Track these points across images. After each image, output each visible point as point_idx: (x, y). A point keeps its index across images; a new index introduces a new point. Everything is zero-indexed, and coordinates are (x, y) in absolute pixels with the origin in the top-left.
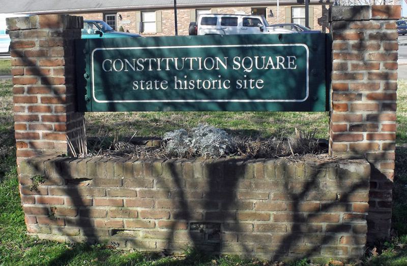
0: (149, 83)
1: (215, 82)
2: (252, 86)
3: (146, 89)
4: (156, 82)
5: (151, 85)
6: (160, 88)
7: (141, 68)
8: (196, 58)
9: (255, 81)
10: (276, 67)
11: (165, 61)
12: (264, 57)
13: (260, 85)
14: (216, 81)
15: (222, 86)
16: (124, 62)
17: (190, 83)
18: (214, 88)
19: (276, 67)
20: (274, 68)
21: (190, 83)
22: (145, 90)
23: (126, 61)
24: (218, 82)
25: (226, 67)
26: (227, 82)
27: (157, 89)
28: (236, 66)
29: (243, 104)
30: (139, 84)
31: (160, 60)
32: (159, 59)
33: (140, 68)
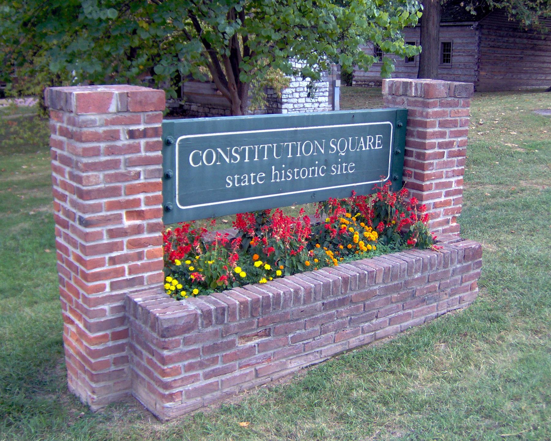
0: (245, 177)
1: (312, 170)
2: (254, 182)
3: (241, 186)
4: (252, 175)
5: (247, 179)
6: (257, 183)
7: (236, 159)
8: (270, 145)
9: (256, 176)
10: (366, 147)
11: (264, 148)
12: (228, 148)
13: (261, 179)
14: (313, 168)
15: (318, 173)
16: (314, 144)
17: (288, 174)
18: (310, 176)
19: (366, 147)
20: (364, 149)
21: (288, 174)
22: (276, 182)
23: (219, 150)
24: (315, 169)
25: (323, 151)
26: (323, 168)
27: (253, 183)
28: (333, 149)
29: (93, 212)
30: (337, 169)
31: (259, 147)
32: (256, 147)
33: (236, 159)
